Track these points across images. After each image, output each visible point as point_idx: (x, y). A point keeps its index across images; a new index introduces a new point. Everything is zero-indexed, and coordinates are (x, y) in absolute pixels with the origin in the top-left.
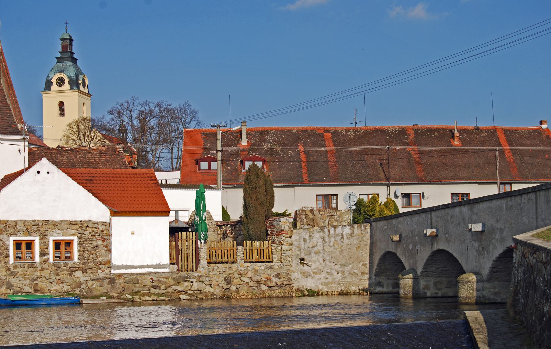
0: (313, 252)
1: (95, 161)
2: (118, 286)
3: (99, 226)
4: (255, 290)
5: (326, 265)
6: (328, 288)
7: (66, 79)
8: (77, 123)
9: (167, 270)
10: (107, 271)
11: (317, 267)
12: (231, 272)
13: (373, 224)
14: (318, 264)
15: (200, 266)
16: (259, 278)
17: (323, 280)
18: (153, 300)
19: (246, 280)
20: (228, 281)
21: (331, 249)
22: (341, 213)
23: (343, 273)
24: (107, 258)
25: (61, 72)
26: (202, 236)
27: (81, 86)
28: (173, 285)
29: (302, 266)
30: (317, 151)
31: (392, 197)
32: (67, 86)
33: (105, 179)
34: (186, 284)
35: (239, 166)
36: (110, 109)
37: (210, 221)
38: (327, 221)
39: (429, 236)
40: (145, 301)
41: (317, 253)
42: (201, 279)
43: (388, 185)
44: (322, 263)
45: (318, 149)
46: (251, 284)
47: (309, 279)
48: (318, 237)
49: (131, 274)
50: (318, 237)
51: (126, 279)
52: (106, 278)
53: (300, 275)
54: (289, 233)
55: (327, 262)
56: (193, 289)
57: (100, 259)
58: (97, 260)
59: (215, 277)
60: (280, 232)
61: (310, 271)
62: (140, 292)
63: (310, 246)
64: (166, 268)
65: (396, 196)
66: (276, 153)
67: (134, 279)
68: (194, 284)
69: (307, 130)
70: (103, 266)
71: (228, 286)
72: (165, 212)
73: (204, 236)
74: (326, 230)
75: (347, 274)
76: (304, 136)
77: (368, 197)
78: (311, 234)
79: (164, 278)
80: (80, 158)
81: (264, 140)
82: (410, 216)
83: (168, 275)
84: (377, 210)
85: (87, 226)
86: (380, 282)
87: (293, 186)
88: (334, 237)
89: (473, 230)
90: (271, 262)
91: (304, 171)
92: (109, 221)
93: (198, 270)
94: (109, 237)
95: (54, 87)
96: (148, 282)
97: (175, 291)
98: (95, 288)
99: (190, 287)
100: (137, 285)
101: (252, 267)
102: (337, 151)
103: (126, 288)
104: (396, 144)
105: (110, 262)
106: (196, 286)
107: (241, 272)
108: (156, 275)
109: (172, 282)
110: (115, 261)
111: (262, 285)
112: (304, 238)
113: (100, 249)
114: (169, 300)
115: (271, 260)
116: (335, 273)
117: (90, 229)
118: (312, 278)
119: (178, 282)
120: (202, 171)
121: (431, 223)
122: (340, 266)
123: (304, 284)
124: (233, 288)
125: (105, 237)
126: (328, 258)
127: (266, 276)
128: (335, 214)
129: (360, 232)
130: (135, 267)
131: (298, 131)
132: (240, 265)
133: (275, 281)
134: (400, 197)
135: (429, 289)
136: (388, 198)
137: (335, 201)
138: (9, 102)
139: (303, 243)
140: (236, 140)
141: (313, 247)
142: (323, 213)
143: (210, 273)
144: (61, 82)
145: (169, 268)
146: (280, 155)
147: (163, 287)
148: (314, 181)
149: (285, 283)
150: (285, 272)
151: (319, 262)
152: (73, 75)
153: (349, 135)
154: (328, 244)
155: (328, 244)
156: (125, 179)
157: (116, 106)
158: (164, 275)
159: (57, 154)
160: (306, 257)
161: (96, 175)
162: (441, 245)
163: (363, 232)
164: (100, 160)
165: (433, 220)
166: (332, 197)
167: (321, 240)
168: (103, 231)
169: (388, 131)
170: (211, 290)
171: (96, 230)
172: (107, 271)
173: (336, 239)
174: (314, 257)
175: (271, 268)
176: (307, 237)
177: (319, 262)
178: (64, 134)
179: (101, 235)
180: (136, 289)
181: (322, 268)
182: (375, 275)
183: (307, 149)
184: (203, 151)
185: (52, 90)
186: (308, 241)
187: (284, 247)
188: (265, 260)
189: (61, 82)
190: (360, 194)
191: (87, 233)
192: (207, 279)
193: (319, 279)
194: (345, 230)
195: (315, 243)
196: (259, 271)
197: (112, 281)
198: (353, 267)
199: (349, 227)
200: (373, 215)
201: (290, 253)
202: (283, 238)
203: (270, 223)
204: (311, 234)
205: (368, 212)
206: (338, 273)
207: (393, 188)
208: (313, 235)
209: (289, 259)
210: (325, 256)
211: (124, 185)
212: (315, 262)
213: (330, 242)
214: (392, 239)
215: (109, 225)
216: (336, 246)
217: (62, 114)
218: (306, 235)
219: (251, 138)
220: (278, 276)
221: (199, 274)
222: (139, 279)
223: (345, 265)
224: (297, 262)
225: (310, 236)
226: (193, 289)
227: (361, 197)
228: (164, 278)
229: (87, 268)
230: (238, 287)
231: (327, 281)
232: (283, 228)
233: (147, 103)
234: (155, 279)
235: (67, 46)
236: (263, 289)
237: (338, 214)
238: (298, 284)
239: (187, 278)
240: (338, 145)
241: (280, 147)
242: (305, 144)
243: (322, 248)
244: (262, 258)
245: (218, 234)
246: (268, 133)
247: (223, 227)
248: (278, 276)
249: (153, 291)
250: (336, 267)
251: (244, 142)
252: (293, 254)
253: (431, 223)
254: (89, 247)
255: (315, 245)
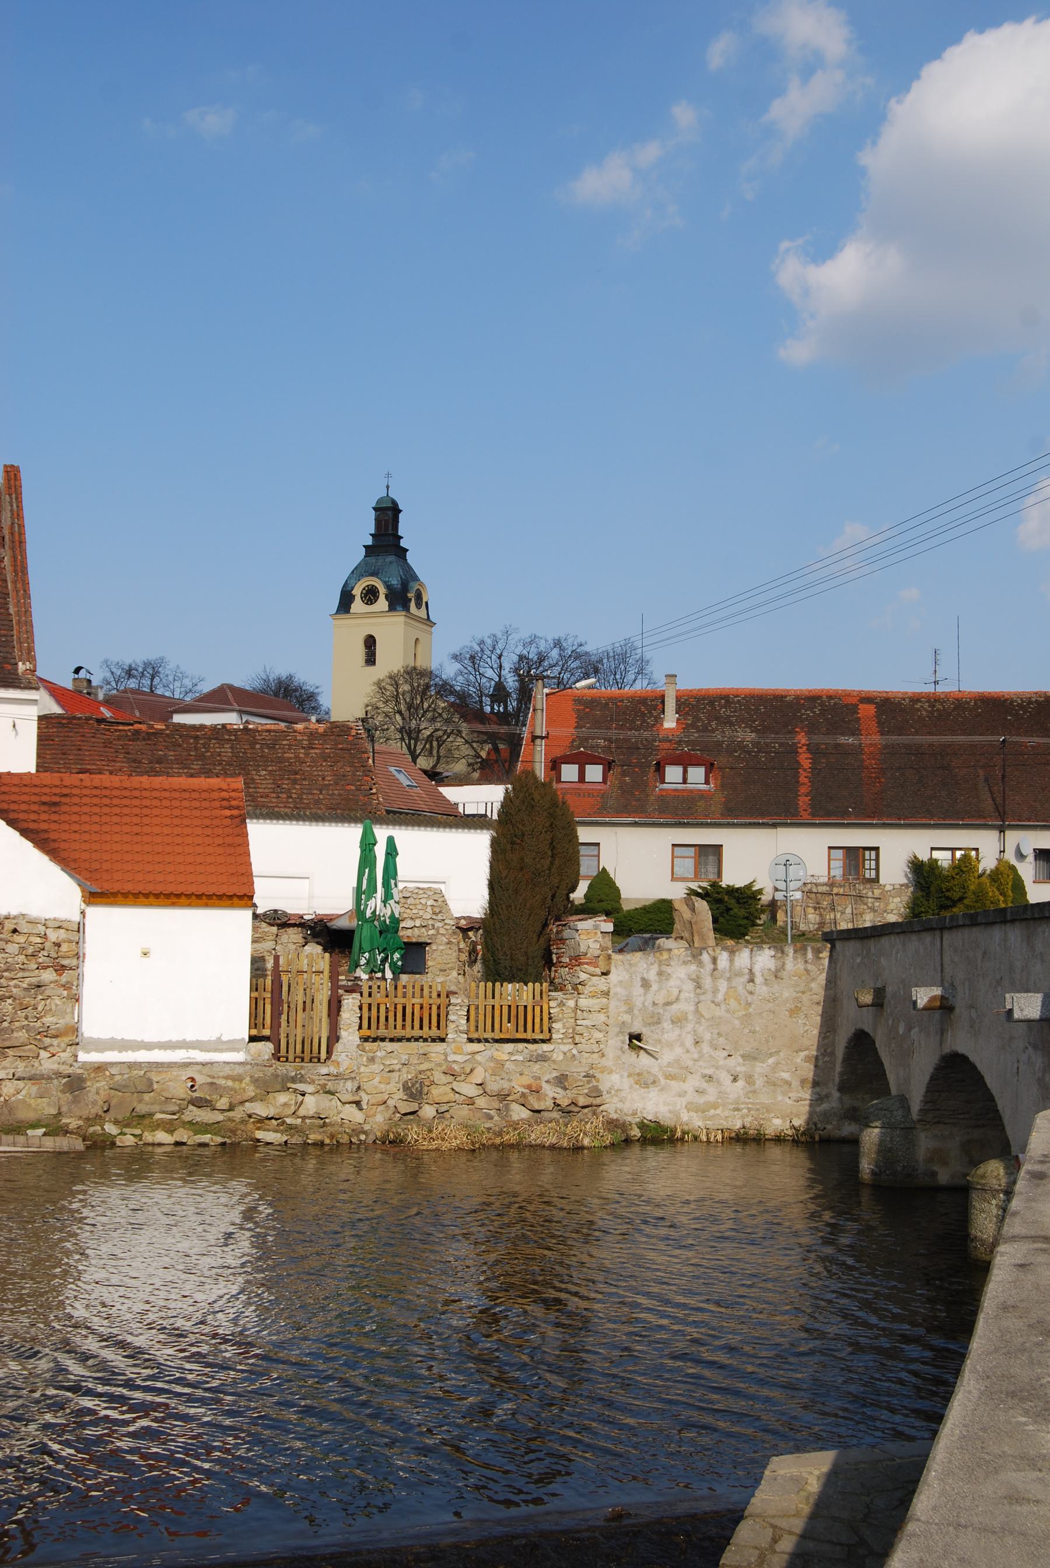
0: (667, 1016)
1: (296, 757)
2: (92, 1096)
3: (49, 932)
4: (491, 1118)
5: (701, 1056)
6: (705, 1119)
7: (382, 591)
8: (393, 678)
9: (239, 1057)
10: (65, 1056)
11: (677, 1061)
12: (424, 1066)
13: (838, 944)
14: (678, 1051)
15: (339, 1047)
16: (506, 1085)
17: (691, 1096)
18: (178, 1144)
19: (468, 1089)
20: (415, 1091)
21: (719, 1012)
22: (884, 893)
23: (750, 1079)
24: (68, 1018)
25: (372, 575)
26: (363, 961)
27: (413, 604)
28: (251, 1100)
29: (634, 1054)
30: (838, 746)
31: (1010, 857)
32: (382, 604)
33: (96, 801)
34: (283, 1098)
35: (651, 775)
36: (456, 650)
37: (439, 917)
38: (849, 910)
39: (925, 1009)
40: (153, 1145)
41: (678, 1021)
42: (330, 1086)
43: (1002, 830)
44: (692, 1049)
45: (843, 740)
46: (481, 1102)
47: (653, 1094)
48: (683, 976)
49: (131, 1066)
50: (683, 976)
51: (118, 1078)
52: (59, 1075)
53: (625, 1080)
54: (601, 962)
55: (706, 1048)
56: (302, 1112)
57: (48, 1020)
58: (38, 1024)
59: (377, 1079)
60: (577, 960)
61: (655, 1070)
62: (151, 1115)
63: (661, 999)
64: (238, 1050)
65: (1020, 856)
66: (741, 746)
67: (141, 1080)
68: (307, 1098)
69: (819, 697)
70: (55, 1042)
71: (414, 1107)
72: (241, 897)
73: (367, 963)
74: (705, 957)
75: (759, 1082)
76: (811, 709)
77: (953, 855)
78: (664, 968)
79: (227, 1078)
80: (261, 748)
81: (717, 719)
82: (902, 936)
83: (240, 1070)
84: (972, 887)
85: (15, 931)
86: (855, 1109)
87: (774, 826)
88: (729, 979)
89: (1017, 1015)
90: (543, 1041)
91: (803, 790)
92: (76, 917)
93: (333, 1057)
94: (74, 962)
95: (358, 606)
96: (180, 1090)
97: (250, 1116)
98: (24, 1101)
99: (293, 1109)
100: (146, 1097)
101: (488, 1053)
102: (886, 746)
103: (114, 1102)
104: (1029, 732)
105: (75, 1030)
106: (311, 1104)
107: (456, 1067)
108: (206, 1070)
109: (251, 1091)
110: (90, 1029)
111: (515, 1107)
112: (643, 979)
113: (48, 992)
114: (223, 1144)
115: (545, 1036)
116: (725, 1078)
117: (21, 939)
118: (662, 1090)
119: (267, 1088)
120: (589, 786)
121: (942, 965)
122: (741, 1060)
123: (639, 1105)
124: (428, 1112)
125: (65, 962)
126: (707, 1036)
127: (526, 1080)
128: (870, 894)
129: (801, 966)
130: (149, 1046)
131: (798, 698)
132: (456, 1049)
133: (551, 1094)
134: (1031, 858)
135: (945, 1163)
136: (999, 860)
137: (873, 863)
138: (12, 611)
139: (641, 991)
140: (652, 716)
141: (668, 1004)
142: (841, 891)
143: (362, 1069)
144: (370, 595)
145: (248, 1051)
146: (749, 753)
147: (223, 1103)
148: (827, 811)
149: (582, 1101)
150: (583, 1070)
151: (682, 1045)
152: (395, 582)
153: (919, 710)
154: (709, 996)
155: (709, 996)
156: (156, 803)
157: (469, 644)
158: (227, 1071)
159: (210, 739)
160: (645, 1032)
161: (75, 791)
162: (961, 1042)
163: (809, 967)
164: (307, 755)
165: (947, 959)
166: (867, 853)
167: (690, 986)
168: (58, 945)
169: (1012, 702)
170: (358, 1116)
171: (39, 940)
172: (65, 1056)
173: (734, 984)
174: (670, 1032)
175: (543, 1058)
176: (652, 975)
177: (682, 1045)
178: (366, 701)
179: (54, 955)
180: (142, 1109)
181: (690, 1063)
182: (841, 1089)
183: (817, 739)
184: (574, 740)
185: (352, 611)
186: (655, 987)
187: (583, 1002)
188: (529, 1035)
189: (370, 595)
190: (932, 849)
191: (12, 948)
192: (349, 1085)
193: (682, 1094)
194: (759, 958)
195: (675, 992)
196: (508, 1065)
197: (75, 1084)
198: (778, 1063)
199: (773, 953)
200: (961, 899)
201: (602, 1017)
202: (583, 976)
203: (558, 932)
204: (664, 968)
205: (948, 890)
206: (735, 1080)
207: (1013, 837)
208: (669, 970)
209: (599, 1035)
210: (700, 1029)
211: (146, 820)
212: (670, 1046)
213: (715, 991)
214: (857, 999)
215: (80, 928)
216: (733, 1003)
217: (371, 660)
218: (648, 970)
219: (687, 714)
220: (561, 1081)
221: (333, 1070)
222: (155, 1079)
223: (755, 1059)
224: (619, 1044)
225: (660, 973)
226: (302, 1112)
227: (936, 855)
228: (227, 1078)
229: (7, 1044)
230: (444, 1108)
231: (701, 1100)
232: (583, 949)
233: (533, 640)
234: (200, 1079)
235: (387, 522)
236: (515, 1117)
237: (877, 892)
238: (619, 1105)
239: (293, 1080)
240: (889, 733)
241: (753, 735)
242: (812, 729)
243: (692, 1008)
244: (521, 1028)
245: (460, 950)
246: (728, 701)
247: (471, 934)
248: (561, 1081)
249: (195, 1114)
250: (731, 1062)
251: (670, 722)
252: (611, 1022)
253: (942, 965)
254: (16, 986)
255: (674, 998)
